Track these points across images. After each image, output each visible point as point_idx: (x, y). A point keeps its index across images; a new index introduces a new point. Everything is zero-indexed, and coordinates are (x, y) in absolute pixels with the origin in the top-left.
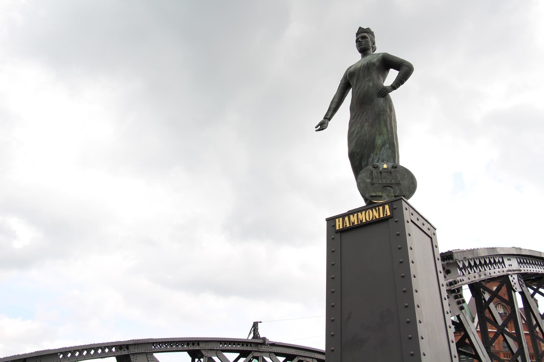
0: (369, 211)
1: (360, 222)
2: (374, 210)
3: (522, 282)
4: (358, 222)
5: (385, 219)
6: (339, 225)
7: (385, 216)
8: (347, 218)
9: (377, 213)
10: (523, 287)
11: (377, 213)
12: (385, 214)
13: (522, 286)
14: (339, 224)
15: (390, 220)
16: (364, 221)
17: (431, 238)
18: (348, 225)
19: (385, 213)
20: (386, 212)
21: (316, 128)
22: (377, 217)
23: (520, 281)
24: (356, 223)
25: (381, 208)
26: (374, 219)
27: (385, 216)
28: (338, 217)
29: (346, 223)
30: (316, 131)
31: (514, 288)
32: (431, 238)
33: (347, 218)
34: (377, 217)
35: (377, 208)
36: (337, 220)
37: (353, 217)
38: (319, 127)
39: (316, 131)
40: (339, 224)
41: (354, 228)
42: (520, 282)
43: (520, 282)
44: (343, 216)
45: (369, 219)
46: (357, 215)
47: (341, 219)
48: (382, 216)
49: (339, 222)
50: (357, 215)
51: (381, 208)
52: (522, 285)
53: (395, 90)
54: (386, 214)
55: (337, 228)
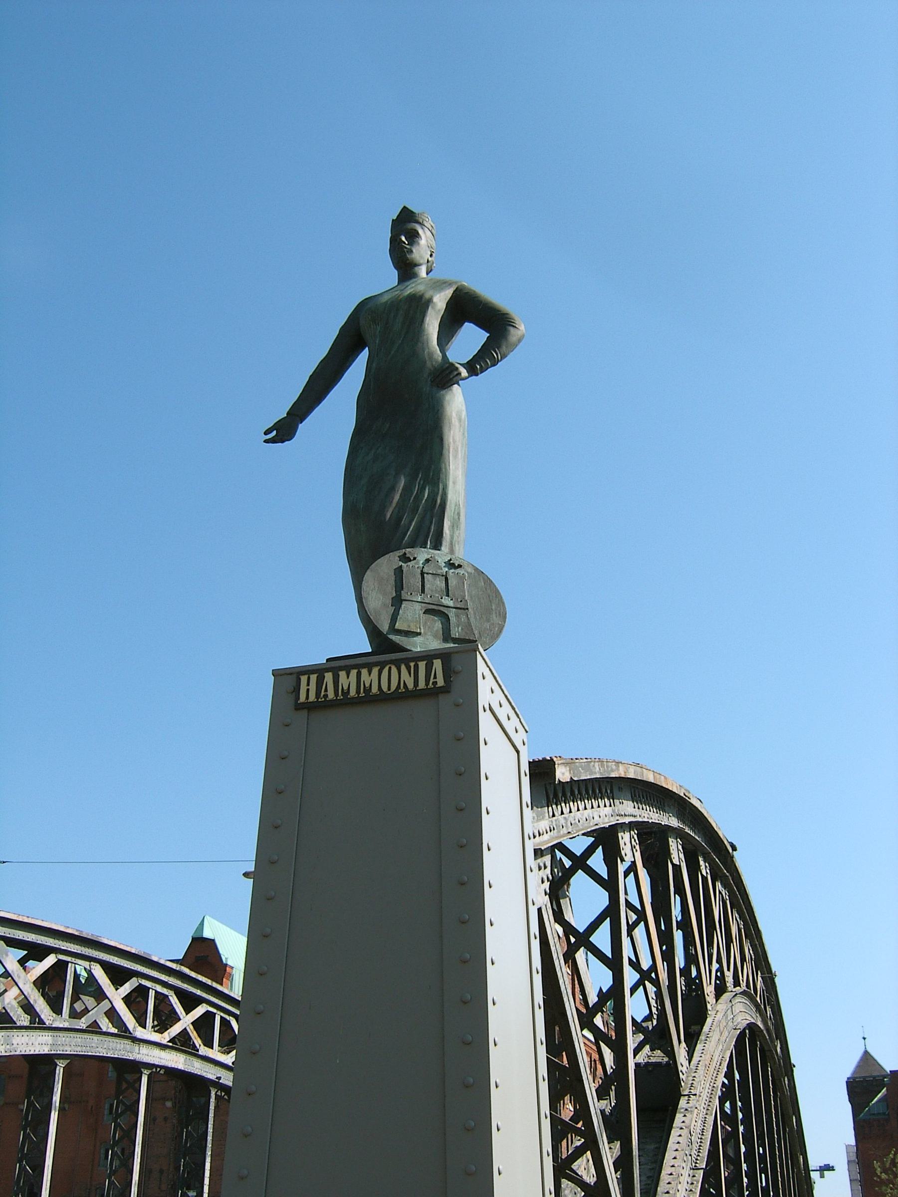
0: (390, 668)
1: (364, 692)
2: (403, 667)
3: (635, 840)
4: (358, 692)
5: (433, 693)
6: (308, 690)
7: (431, 685)
8: (329, 677)
9: (364, 682)
10: (636, 851)
11: (364, 682)
12: (431, 682)
13: (634, 850)
14: (308, 690)
15: (441, 697)
16: (375, 689)
17: (518, 752)
18: (331, 695)
19: (432, 680)
20: (435, 677)
21: (266, 433)
22: (411, 686)
23: (633, 837)
24: (353, 693)
25: (422, 665)
26: (402, 689)
27: (431, 685)
28: (307, 671)
29: (326, 690)
30: (266, 441)
31: (623, 853)
32: (518, 752)
33: (329, 677)
34: (411, 686)
35: (412, 664)
36: (304, 679)
37: (346, 677)
38: (274, 433)
39: (266, 441)
40: (308, 690)
41: (344, 702)
42: (633, 840)
43: (633, 840)
44: (319, 671)
45: (389, 689)
46: (359, 675)
47: (314, 678)
48: (422, 685)
49: (308, 684)
50: (359, 675)
51: (422, 665)
52: (635, 847)
53: (474, 377)
54: (433, 682)
55: (302, 698)
